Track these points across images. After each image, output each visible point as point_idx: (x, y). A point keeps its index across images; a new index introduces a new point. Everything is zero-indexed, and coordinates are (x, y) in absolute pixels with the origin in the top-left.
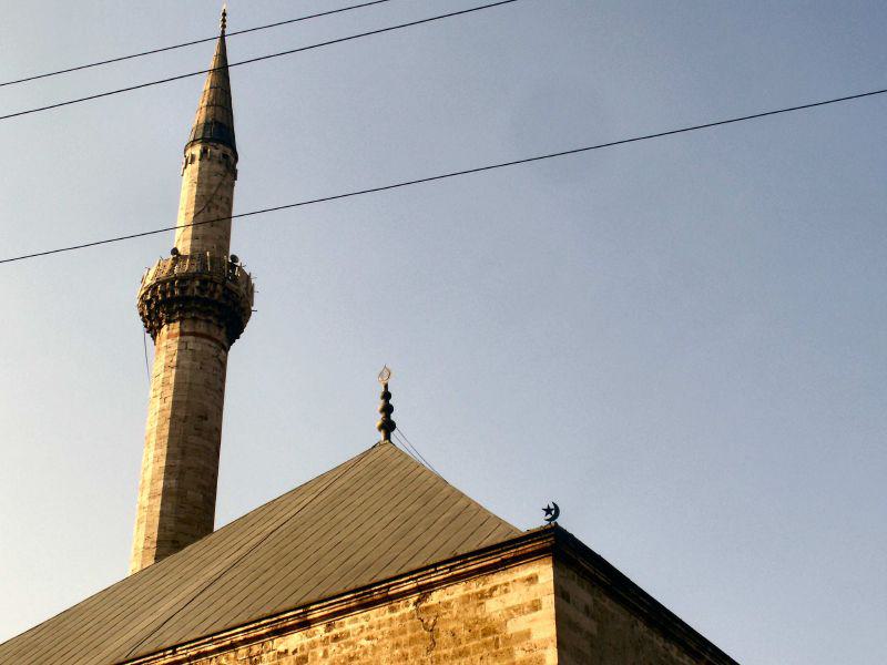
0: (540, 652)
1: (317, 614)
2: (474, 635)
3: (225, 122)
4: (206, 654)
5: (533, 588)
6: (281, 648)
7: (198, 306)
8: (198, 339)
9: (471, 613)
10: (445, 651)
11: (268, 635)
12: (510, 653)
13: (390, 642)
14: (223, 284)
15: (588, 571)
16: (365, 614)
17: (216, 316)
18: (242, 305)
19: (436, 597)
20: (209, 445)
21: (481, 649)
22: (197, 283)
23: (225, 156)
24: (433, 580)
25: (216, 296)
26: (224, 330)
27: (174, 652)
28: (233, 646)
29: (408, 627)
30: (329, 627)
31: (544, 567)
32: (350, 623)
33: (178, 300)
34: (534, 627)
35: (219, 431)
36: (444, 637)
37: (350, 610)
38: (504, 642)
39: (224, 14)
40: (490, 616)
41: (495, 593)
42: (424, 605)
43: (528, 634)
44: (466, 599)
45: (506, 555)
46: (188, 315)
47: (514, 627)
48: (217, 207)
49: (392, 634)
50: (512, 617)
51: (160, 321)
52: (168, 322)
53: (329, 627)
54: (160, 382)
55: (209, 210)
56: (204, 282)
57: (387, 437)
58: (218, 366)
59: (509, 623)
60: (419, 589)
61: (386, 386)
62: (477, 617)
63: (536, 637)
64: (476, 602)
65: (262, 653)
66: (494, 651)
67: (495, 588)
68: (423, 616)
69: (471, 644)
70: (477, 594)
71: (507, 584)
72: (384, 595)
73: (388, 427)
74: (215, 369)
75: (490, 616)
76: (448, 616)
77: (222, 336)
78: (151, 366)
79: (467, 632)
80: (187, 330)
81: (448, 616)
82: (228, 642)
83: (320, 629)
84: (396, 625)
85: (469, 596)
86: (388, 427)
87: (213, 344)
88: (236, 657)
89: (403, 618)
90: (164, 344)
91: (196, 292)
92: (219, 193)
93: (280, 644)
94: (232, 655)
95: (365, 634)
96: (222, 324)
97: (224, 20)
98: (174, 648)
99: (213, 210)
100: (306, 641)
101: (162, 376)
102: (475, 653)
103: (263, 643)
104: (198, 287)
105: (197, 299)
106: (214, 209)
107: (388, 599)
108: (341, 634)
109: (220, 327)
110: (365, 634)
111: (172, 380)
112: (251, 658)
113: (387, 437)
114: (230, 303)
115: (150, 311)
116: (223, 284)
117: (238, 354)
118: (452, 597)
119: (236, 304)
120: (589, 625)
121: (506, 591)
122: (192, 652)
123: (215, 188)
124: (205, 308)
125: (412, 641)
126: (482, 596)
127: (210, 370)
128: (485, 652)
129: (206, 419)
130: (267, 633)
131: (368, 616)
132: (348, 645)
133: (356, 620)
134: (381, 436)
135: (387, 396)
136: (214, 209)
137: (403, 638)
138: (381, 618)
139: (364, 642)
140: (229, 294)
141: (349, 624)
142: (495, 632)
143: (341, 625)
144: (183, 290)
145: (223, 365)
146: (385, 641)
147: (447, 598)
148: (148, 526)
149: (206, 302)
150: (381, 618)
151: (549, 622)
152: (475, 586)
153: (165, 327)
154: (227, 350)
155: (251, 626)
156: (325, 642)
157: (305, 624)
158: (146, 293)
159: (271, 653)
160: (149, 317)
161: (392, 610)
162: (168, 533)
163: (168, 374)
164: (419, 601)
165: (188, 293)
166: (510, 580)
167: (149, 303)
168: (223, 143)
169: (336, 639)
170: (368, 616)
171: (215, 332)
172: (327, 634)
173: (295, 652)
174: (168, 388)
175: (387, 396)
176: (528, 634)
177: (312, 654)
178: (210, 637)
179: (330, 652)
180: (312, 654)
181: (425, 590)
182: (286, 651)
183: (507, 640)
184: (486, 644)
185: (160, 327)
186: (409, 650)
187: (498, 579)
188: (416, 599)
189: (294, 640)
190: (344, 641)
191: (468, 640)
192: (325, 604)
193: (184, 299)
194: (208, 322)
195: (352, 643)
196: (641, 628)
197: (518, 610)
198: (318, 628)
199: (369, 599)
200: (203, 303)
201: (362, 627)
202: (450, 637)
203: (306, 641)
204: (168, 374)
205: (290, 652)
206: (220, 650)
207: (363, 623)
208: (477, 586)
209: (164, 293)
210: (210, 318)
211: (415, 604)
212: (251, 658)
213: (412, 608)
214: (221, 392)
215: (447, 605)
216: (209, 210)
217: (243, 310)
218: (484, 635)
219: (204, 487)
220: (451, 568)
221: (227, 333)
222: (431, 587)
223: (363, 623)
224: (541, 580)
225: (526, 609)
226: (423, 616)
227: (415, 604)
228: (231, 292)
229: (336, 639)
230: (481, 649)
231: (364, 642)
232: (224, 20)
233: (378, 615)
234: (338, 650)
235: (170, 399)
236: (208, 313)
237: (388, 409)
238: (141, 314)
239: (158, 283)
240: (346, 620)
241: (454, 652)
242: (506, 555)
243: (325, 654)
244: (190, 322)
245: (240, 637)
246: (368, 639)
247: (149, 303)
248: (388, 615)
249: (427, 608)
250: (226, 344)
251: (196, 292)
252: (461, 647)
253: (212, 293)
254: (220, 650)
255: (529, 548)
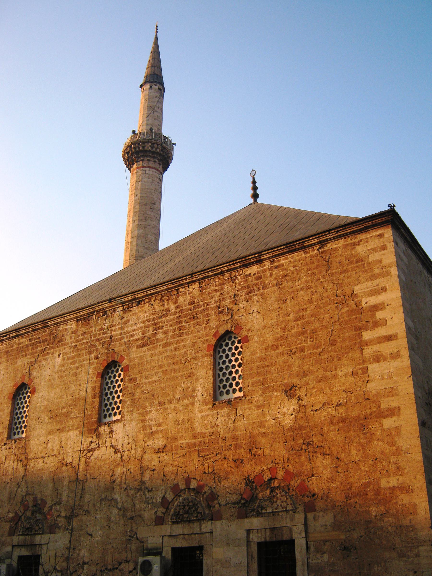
0: (388, 269)
1: (266, 256)
2: (351, 263)
3: (159, 74)
4: (208, 277)
5: (381, 239)
6: (247, 273)
7: (150, 154)
8: (151, 169)
9: (349, 252)
10: (336, 271)
11: (240, 267)
12: (372, 270)
13: (305, 268)
14: (161, 145)
15: (403, 234)
16: (291, 256)
17: (158, 160)
18: (169, 155)
19: (328, 246)
20: (157, 216)
21: (355, 269)
22: (150, 144)
23: (159, 89)
24: (328, 238)
25: (158, 150)
26: (161, 166)
27: (192, 276)
28: (222, 273)
29: (315, 261)
30: (272, 262)
31: (388, 230)
32: (283, 260)
33: (141, 151)
34: (383, 258)
35: (160, 210)
36: (335, 264)
37: (283, 254)
38: (367, 265)
39: (157, 27)
40: (359, 253)
41: (361, 243)
42: (323, 250)
43: (381, 261)
44: (345, 246)
45: (366, 225)
46: (146, 159)
47: (372, 258)
48: (157, 112)
49: (307, 264)
50: (371, 253)
51: (133, 161)
52: (137, 162)
53: (272, 262)
54: (134, 188)
55: (153, 113)
56: (153, 144)
57: (255, 200)
58: (159, 181)
59: (370, 256)
60: (320, 242)
61: (254, 178)
62: (352, 254)
63: (385, 262)
64: (351, 247)
65: (237, 275)
66: (363, 269)
67: (361, 241)
68: (322, 255)
69: (350, 267)
70: (351, 244)
71: (367, 238)
72: (302, 246)
73: (255, 196)
74: (158, 183)
75: (359, 253)
76: (337, 254)
77: (161, 169)
78: (120, 183)
79: (347, 261)
80: (145, 165)
81: (337, 254)
82: (220, 271)
83: (267, 264)
84: (308, 260)
85: (347, 245)
86: (255, 196)
87: (157, 172)
88: (223, 278)
89: (312, 256)
90: (135, 171)
91: (150, 148)
92: (157, 105)
93: (247, 271)
94: (221, 277)
95: (292, 265)
96: (160, 163)
97: (157, 29)
98: (191, 275)
99: (155, 113)
100: (260, 269)
101: (135, 185)
102: (352, 271)
103: (237, 271)
104: (150, 146)
105: (150, 151)
106: (154, 110)
107: (304, 248)
108: (279, 265)
109: (160, 164)
110: (292, 265)
111: (139, 187)
112: (232, 278)
113: (255, 200)
114: (164, 154)
115: (128, 157)
116: (161, 145)
117: (167, 176)
118: (338, 245)
119: (167, 154)
120: (405, 259)
121: (367, 242)
122: (201, 277)
123: (155, 103)
124: (153, 156)
125: (317, 267)
126: (354, 245)
127: (156, 183)
128: (358, 270)
129: (155, 204)
130: (240, 266)
131: (293, 256)
132: (283, 270)
133: (287, 259)
134: (252, 201)
135: (254, 182)
136: (154, 110)
137: (313, 266)
138: (300, 257)
139: (292, 269)
140: (163, 149)
141: (282, 261)
142: (362, 261)
143: (279, 261)
144: (143, 147)
145: (161, 181)
146: (303, 267)
147: (335, 246)
148: (131, 250)
149: (153, 153)
150: (300, 257)
151: (392, 255)
152: (350, 240)
153: (136, 164)
154: (162, 175)
155: (231, 263)
156: (271, 269)
157: (259, 261)
158: (127, 149)
159: (242, 275)
160: (128, 160)
161: (306, 253)
162: (140, 253)
163: (137, 184)
164: (320, 248)
165: (146, 148)
166: (368, 236)
167: (128, 153)
168: (159, 83)
169: (276, 267)
170: (293, 256)
171: (158, 166)
172: (272, 265)
173: (255, 274)
174: (138, 190)
175: (254, 182)
176: (381, 261)
177: (264, 275)
178: (209, 269)
179: (273, 273)
180: (264, 275)
181: (323, 243)
182: (250, 274)
183: (369, 264)
184: (358, 267)
185: (133, 164)
186: (316, 271)
187: (363, 236)
188: (318, 247)
189: (254, 269)
190: (281, 268)
191: (348, 265)
192: (270, 251)
193: (137, 153)
194: (155, 162)
195: (286, 269)
196: (420, 266)
197: (375, 250)
198: (267, 263)
199: (294, 248)
200: (150, 153)
201: (290, 261)
202: (338, 264)
203: (260, 269)
204: (137, 184)
205: (252, 274)
206: (215, 275)
207: (291, 260)
208: (351, 240)
209: (135, 148)
210: (156, 160)
211: (318, 249)
212: (232, 278)
213: (316, 251)
214: (161, 192)
215: (336, 249)
216: (153, 113)
217: (170, 157)
218: (357, 262)
219: (155, 234)
220: (337, 232)
221: (163, 167)
222: (326, 241)
223: (291, 260)
224: (386, 236)
225: (379, 249)
226: (322, 255)
227: (318, 249)
228: (164, 148)
229: (276, 267)
230: (355, 269)
231: (292, 269)
232: (157, 29)
233: (298, 256)
234: (277, 272)
235: (139, 195)
236: (154, 158)
237: (255, 188)
238: (124, 158)
239: (132, 144)
240: (281, 259)
241: (341, 271)
242: (366, 225)
243: (271, 275)
244: (147, 161)
245: (226, 269)
246: (294, 267)
247: (128, 153)
248: (303, 255)
249: (324, 251)
250: (162, 172)
251: (150, 148)
252: (345, 268)
253: (156, 149)
254: (215, 275)
255: (379, 220)
